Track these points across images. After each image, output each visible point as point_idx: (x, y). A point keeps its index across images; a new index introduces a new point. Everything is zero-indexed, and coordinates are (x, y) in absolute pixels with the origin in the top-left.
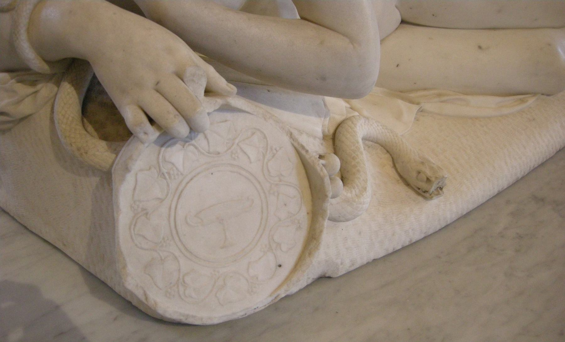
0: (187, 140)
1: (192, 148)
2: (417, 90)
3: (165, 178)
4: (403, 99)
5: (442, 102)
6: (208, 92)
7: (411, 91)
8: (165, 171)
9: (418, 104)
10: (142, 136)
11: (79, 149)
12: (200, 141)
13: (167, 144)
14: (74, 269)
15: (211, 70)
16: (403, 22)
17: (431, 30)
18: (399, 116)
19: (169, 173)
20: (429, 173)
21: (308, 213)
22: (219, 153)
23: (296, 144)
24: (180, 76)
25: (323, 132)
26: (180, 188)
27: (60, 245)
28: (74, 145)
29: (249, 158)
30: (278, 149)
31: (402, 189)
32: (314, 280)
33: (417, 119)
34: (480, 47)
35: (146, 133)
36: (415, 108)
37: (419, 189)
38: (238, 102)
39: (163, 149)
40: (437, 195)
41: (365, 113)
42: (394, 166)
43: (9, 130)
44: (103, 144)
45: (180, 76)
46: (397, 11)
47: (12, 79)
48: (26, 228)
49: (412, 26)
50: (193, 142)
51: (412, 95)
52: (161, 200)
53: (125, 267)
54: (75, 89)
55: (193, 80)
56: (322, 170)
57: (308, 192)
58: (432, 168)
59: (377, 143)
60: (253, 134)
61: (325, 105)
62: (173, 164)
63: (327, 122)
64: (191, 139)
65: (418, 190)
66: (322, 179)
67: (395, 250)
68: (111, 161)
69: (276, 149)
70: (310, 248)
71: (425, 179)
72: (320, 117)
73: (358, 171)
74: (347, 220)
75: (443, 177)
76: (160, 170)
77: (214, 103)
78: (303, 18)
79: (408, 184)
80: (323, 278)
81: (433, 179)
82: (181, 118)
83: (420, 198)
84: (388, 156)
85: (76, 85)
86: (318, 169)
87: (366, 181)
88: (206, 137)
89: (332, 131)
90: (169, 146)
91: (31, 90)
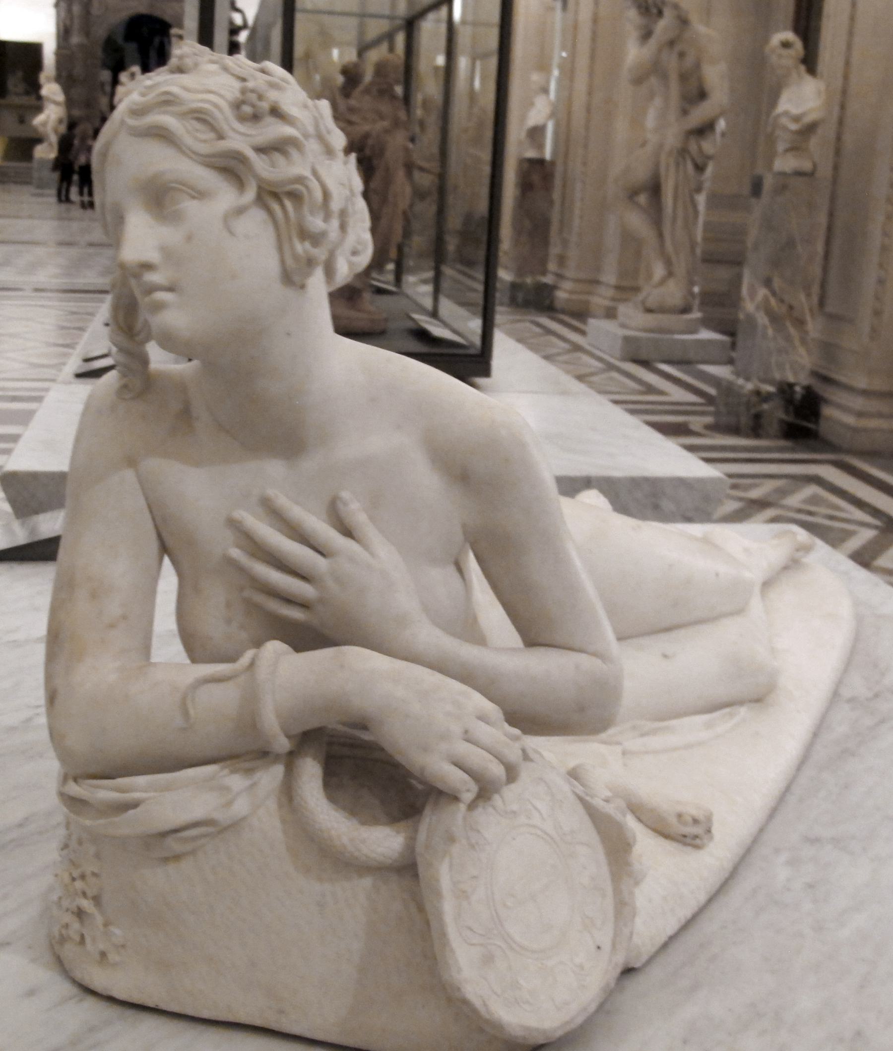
9: (618, 743)
37: (685, 836)
79: (667, 836)
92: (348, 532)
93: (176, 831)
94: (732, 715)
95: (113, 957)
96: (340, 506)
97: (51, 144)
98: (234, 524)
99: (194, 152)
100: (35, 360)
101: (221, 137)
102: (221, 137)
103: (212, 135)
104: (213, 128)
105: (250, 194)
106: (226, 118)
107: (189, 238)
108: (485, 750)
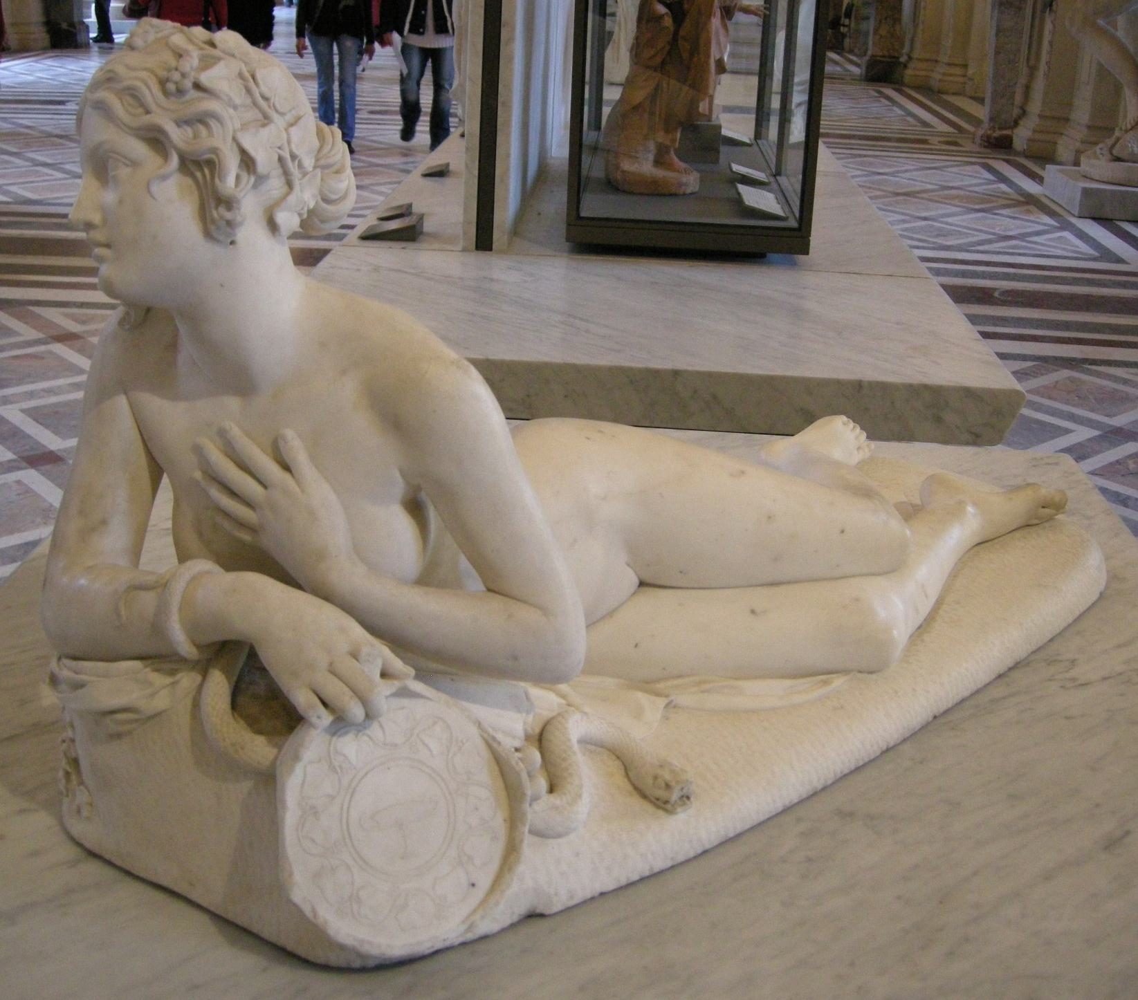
0: (360, 728)
1: (365, 738)
2: (666, 679)
3: (337, 773)
4: (646, 691)
5: (703, 692)
6: (384, 675)
7: (659, 680)
8: (336, 764)
9: (667, 696)
10: (314, 720)
11: (233, 745)
12: (374, 730)
13: (339, 733)
14: (204, 919)
15: (386, 651)
16: (642, 584)
17: (679, 592)
18: (638, 713)
19: (341, 767)
20: (667, 776)
21: (505, 820)
22: (396, 745)
23: (485, 735)
24: (355, 655)
25: (525, 731)
26: (353, 785)
27: (181, 888)
28: (227, 740)
29: (430, 750)
30: (464, 741)
31: (637, 803)
32: (522, 917)
33: (666, 718)
34: (753, 612)
35: (319, 717)
36: (662, 702)
37: (658, 799)
38: (418, 686)
39: (334, 739)
40: (682, 805)
41: (587, 709)
42: (627, 775)
43: (130, 733)
44: (260, 740)
45: (355, 655)
46: (628, 568)
47: (146, 667)
48: (128, 873)
49: (656, 589)
50: (367, 732)
51: (661, 686)
52: (332, 798)
53: (291, 875)
54: (227, 677)
55: (369, 661)
56: (517, 764)
57: (503, 793)
58: (672, 771)
59: (602, 747)
60: (435, 723)
61: (528, 698)
62: (344, 756)
63: (530, 718)
64: (365, 728)
65: (656, 801)
66: (518, 774)
67: (629, 882)
68: (271, 757)
69: (462, 741)
70: (386, 63)
71: (663, 785)
72: (519, 711)
73: (571, 775)
74: (559, 836)
75: (687, 781)
76: (331, 762)
77: (394, 685)
78: (489, 590)
79: (644, 796)
80: (533, 916)
81: (673, 784)
82: (357, 699)
83: (661, 812)
84: (617, 763)
85: (226, 672)
86: (513, 763)
87: (581, 786)
88: (381, 726)
89: (537, 730)
90: (339, 736)
91: (169, 680)
92: (287, 468)
93: (113, 712)
94: (826, 683)
95: (85, 813)
96: (281, 444)
97: (395, 49)
98: (198, 450)
99: (125, 125)
100: (860, 183)
101: (148, 112)
102: (148, 112)
103: (141, 110)
104: (142, 104)
105: (175, 161)
106: (152, 94)
107: (121, 202)
108: (348, 687)
